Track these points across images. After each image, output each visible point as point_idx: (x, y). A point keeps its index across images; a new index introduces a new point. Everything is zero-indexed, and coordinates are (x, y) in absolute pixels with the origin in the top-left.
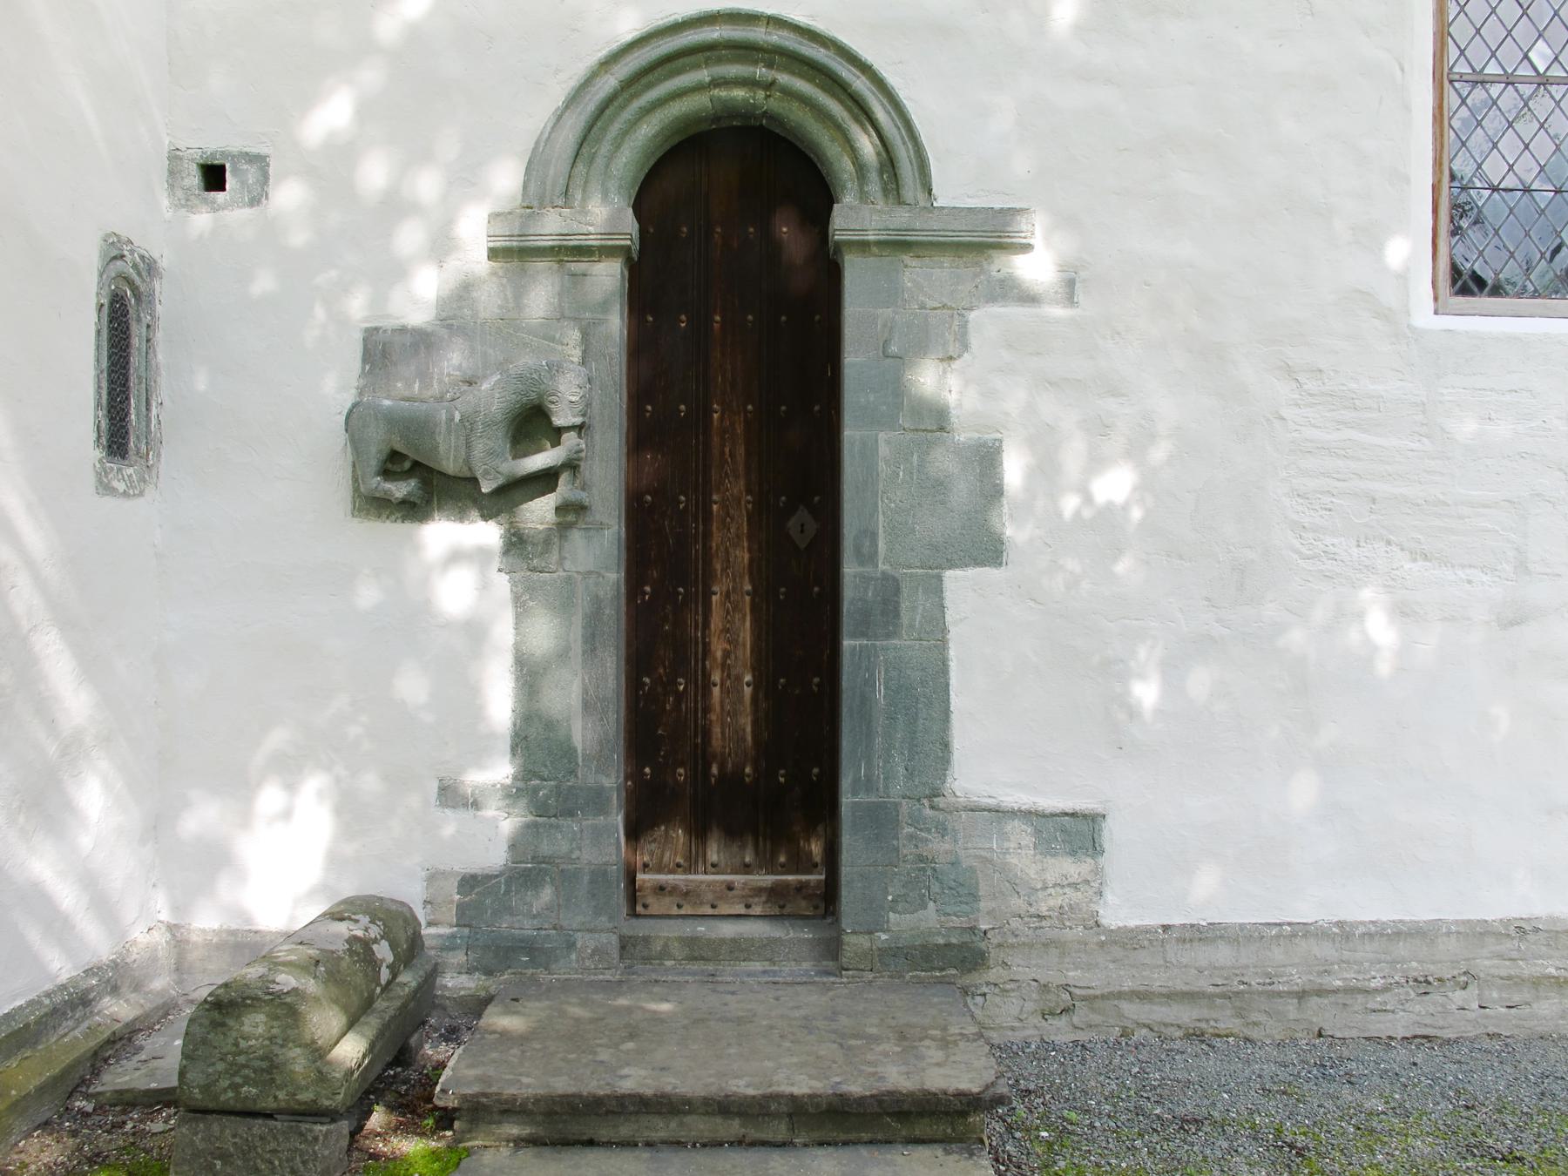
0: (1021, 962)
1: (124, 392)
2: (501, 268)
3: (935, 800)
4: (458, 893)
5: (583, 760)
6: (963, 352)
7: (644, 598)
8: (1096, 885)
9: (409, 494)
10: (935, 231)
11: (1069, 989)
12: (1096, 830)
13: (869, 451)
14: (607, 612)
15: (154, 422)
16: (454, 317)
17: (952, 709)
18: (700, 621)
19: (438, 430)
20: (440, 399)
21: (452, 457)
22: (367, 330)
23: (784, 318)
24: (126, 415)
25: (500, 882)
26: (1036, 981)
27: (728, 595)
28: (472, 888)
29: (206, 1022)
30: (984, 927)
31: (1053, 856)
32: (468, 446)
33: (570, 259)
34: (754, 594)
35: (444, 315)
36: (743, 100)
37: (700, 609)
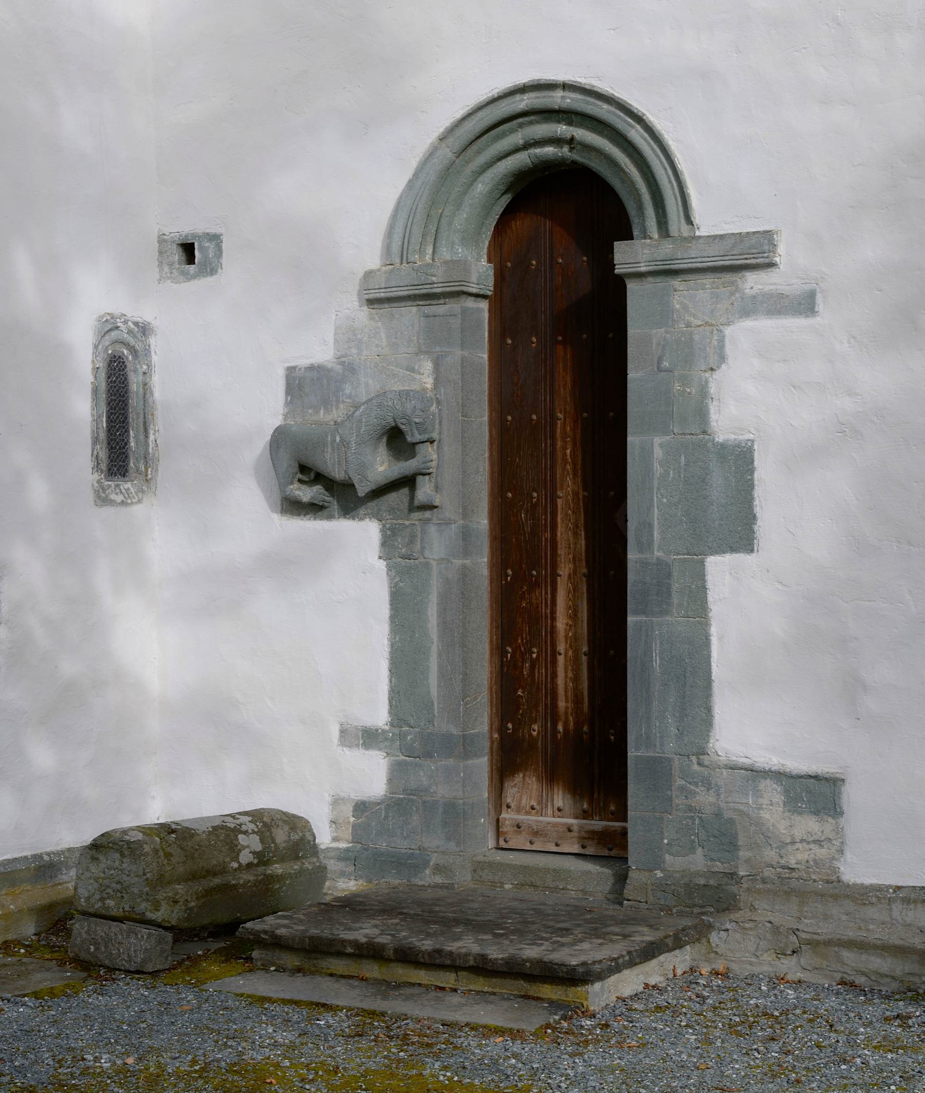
0: (766, 907)
1: (124, 427)
3: (701, 757)
4: (353, 816)
5: (438, 712)
6: (721, 364)
7: (506, 580)
8: (837, 843)
10: (693, 258)
11: (797, 933)
12: (837, 793)
13: (647, 453)
15: (151, 445)
16: (345, 356)
17: (713, 678)
23: (611, 335)
24: (126, 444)
25: (381, 809)
26: (770, 922)
28: (363, 812)
29: (89, 857)
30: (742, 873)
31: (800, 814)
35: (339, 353)
36: (553, 154)
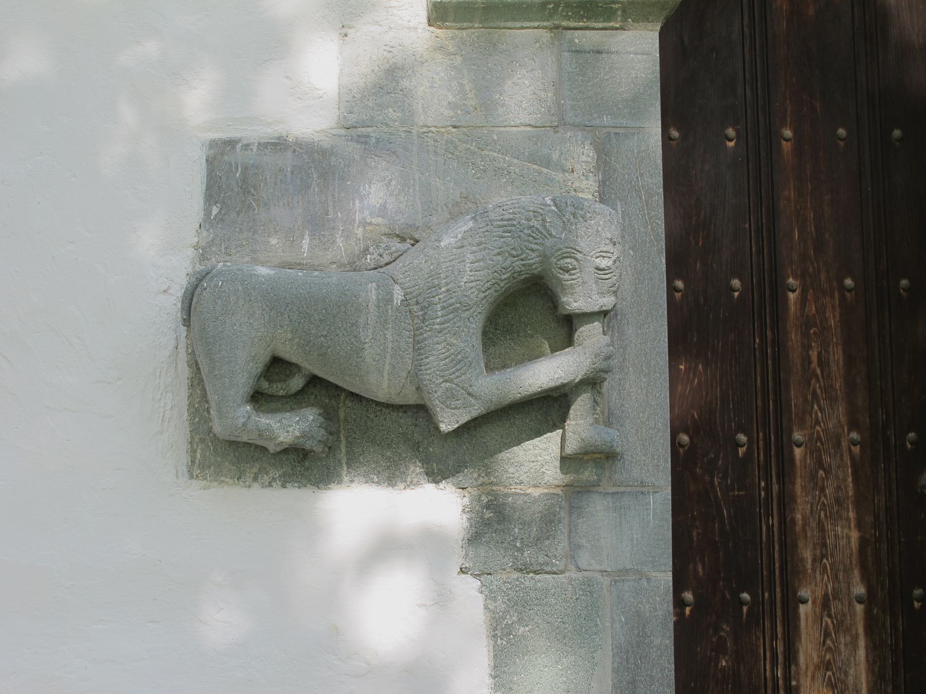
2: (452, 38)
9: (304, 435)
14: (657, 642)
18: (780, 649)
19: (362, 321)
20: (353, 266)
21: (387, 367)
22: (213, 144)
23: (897, 133)
27: (825, 604)
32: (418, 347)
33: (572, 24)
34: (869, 600)
35: (353, 119)
37: (779, 629)
